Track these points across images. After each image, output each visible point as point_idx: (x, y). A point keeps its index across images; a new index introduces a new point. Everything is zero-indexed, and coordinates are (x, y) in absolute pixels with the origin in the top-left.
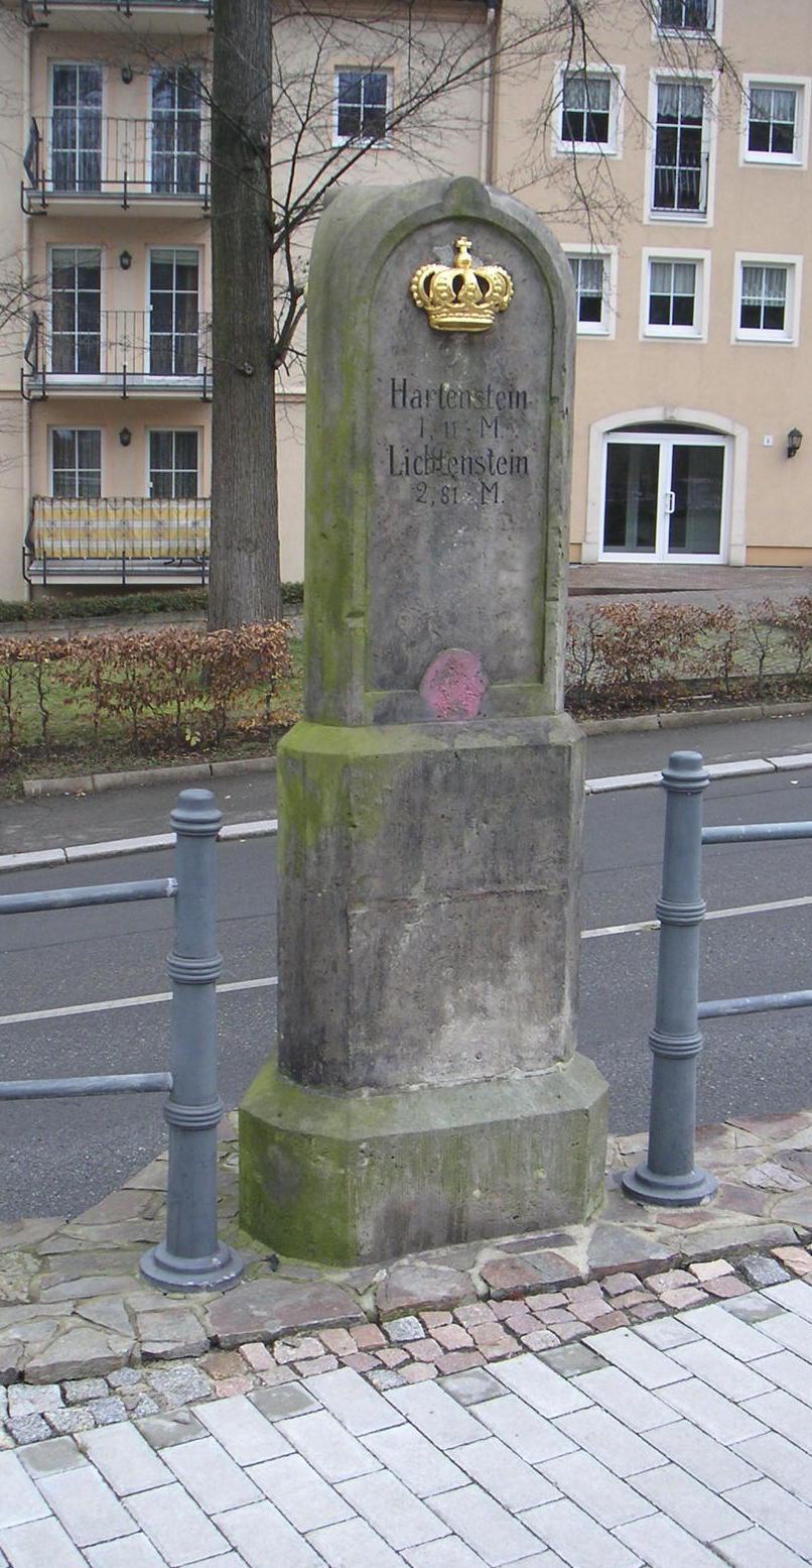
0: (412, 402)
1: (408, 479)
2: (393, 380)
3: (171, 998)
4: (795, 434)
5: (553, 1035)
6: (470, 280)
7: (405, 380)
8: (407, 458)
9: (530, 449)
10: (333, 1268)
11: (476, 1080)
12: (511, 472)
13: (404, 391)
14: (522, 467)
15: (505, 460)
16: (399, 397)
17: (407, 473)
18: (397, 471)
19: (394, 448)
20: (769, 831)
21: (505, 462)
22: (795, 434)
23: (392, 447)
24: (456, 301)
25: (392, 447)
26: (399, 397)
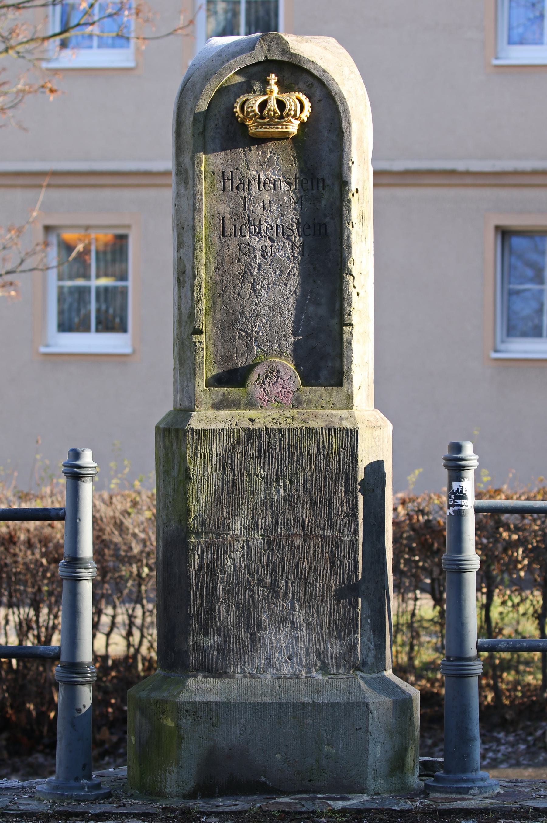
0: (237, 187)
1: (236, 240)
2: (223, 172)
3: (125, 773)
4: (357, 189)
5: (352, 648)
6: (273, 105)
7: (232, 172)
8: (235, 225)
9: (328, 218)
10: (118, 658)
11: (288, 676)
12: (314, 235)
13: (232, 180)
14: (323, 231)
15: (309, 226)
16: (228, 184)
17: (235, 236)
18: (228, 234)
19: (225, 219)
20: (543, 505)
21: (309, 227)
22: (357, 189)
23: (223, 218)
24: (262, 117)
25: (223, 218)
26: (228, 184)
